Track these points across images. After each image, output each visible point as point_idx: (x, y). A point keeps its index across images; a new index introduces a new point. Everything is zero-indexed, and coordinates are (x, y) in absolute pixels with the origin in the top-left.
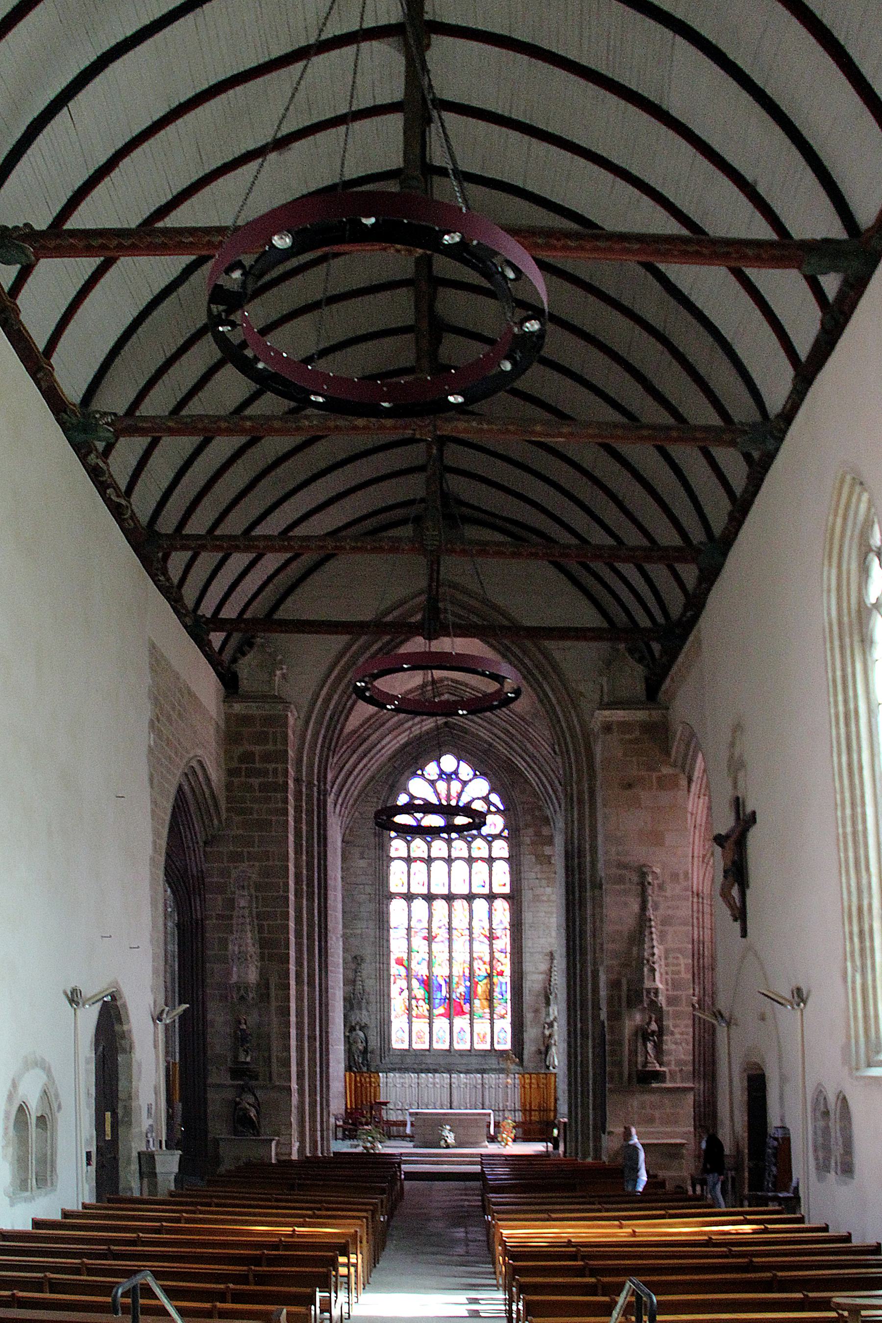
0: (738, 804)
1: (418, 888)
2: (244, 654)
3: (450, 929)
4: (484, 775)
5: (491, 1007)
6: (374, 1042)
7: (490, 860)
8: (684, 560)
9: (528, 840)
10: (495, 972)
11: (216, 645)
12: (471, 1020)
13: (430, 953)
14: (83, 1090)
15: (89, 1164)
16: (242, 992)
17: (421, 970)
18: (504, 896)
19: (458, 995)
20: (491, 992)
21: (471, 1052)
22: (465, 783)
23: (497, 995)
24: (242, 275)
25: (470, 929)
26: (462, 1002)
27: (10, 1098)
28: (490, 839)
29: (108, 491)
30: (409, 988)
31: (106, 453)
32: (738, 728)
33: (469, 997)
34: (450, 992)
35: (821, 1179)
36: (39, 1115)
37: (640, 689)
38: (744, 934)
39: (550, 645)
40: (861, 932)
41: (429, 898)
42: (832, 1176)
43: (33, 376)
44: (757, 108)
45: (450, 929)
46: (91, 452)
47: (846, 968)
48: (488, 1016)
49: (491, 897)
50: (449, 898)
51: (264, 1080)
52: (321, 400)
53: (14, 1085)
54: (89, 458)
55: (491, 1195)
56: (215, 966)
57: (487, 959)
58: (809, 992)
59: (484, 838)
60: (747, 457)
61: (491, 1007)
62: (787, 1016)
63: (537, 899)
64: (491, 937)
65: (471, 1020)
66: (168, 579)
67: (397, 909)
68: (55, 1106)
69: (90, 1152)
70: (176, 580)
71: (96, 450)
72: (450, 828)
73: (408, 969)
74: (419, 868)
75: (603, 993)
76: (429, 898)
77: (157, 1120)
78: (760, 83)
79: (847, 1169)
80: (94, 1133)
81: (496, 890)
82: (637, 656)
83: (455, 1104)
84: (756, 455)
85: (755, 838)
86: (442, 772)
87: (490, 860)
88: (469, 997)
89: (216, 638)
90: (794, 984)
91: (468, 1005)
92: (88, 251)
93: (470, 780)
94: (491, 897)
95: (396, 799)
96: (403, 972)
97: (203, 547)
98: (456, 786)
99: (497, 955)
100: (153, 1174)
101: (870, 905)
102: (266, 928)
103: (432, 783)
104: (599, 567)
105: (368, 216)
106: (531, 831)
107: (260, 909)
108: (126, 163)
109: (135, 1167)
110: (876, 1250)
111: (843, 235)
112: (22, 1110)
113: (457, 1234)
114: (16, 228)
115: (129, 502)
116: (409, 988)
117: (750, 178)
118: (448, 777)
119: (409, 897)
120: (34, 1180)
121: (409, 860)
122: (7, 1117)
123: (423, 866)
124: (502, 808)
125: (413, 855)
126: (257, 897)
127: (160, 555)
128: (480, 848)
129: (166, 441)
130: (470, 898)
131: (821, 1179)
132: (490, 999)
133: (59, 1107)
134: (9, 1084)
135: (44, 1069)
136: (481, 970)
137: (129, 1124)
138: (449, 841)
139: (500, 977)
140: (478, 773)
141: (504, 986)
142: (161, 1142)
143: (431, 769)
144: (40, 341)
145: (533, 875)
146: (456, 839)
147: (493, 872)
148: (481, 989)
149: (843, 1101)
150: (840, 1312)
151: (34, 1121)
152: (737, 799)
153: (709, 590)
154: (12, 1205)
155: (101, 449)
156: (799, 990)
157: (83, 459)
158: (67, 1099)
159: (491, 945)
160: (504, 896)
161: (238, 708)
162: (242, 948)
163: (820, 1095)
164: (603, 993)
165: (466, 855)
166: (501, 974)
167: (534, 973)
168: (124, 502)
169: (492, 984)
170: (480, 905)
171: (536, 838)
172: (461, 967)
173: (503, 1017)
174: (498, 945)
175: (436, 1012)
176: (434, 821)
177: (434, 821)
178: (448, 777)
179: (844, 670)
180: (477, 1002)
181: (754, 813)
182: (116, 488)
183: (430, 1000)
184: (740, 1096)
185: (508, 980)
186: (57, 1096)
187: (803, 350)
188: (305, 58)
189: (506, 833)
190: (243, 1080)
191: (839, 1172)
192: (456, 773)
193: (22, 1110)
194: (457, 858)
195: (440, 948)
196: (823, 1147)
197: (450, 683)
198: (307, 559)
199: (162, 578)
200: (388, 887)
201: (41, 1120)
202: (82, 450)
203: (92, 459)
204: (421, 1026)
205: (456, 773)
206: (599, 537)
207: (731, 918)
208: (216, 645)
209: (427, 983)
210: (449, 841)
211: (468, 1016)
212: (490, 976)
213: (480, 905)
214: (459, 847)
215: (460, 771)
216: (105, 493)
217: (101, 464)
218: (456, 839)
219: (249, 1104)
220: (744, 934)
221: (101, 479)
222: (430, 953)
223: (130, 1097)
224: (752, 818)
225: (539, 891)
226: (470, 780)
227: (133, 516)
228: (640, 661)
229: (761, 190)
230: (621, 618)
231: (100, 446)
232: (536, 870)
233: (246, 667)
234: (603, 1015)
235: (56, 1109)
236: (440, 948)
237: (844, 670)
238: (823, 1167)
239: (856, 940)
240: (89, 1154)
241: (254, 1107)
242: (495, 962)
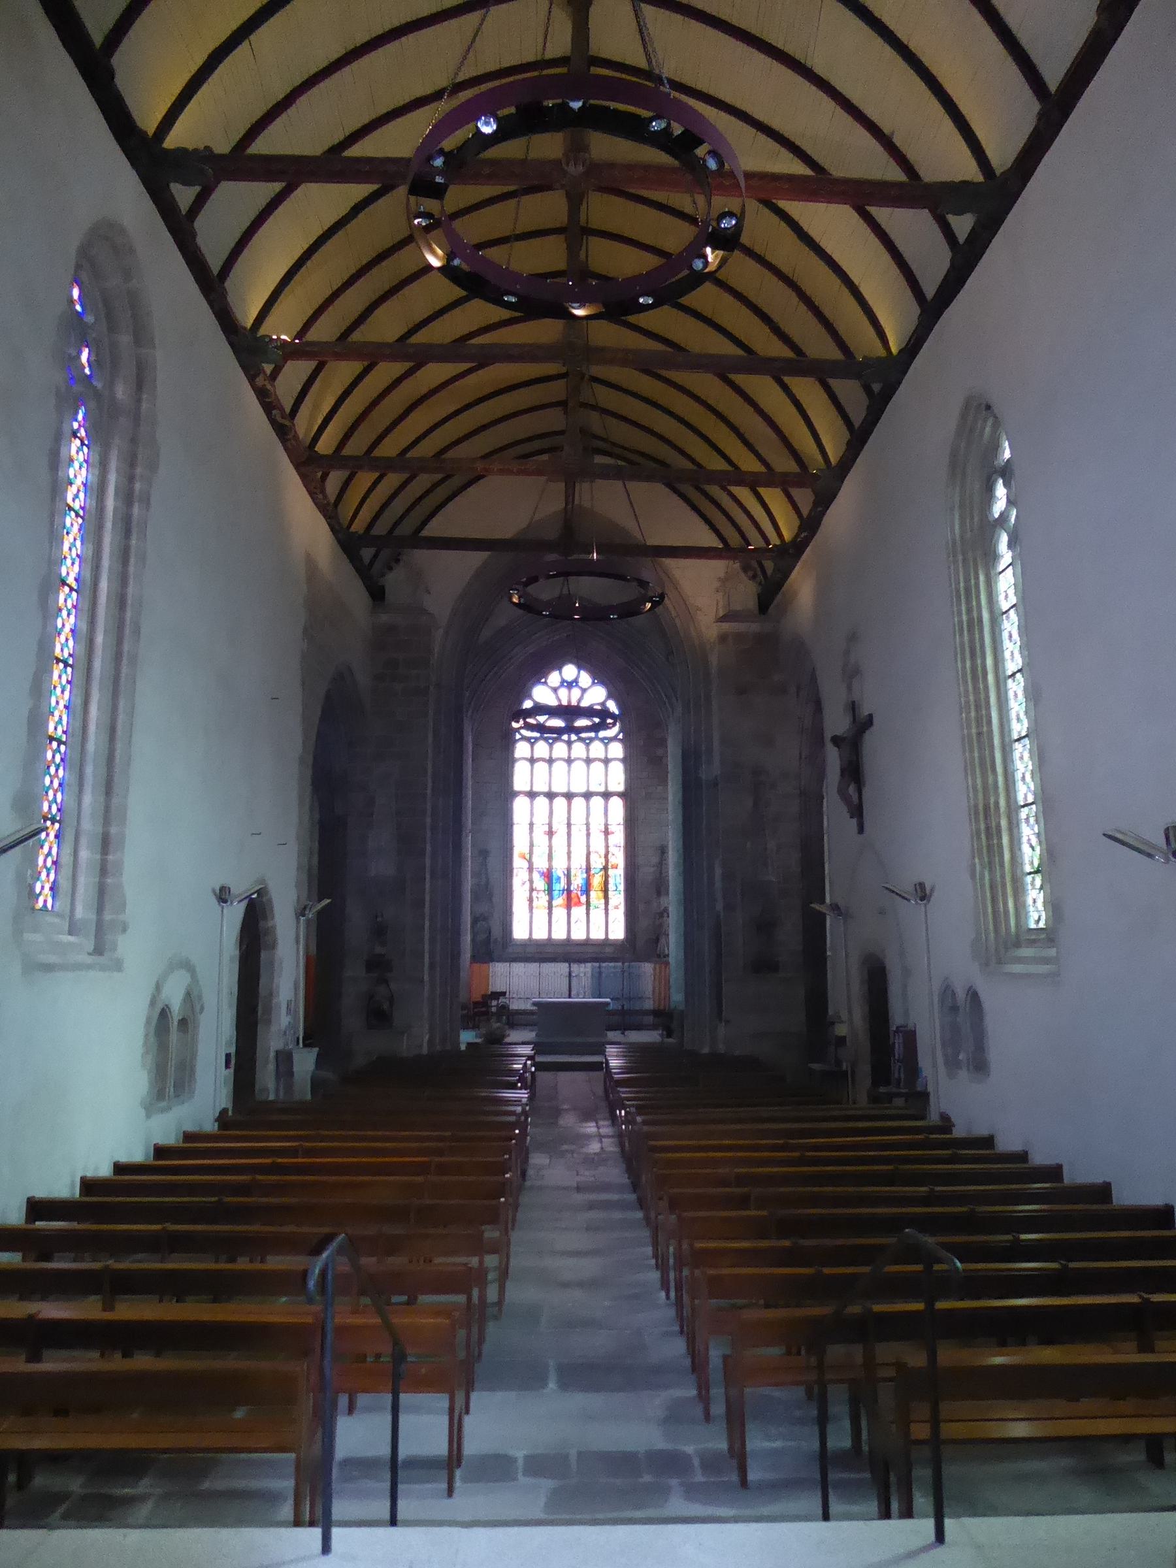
0: (853, 707)
1: (557, 788)
2: (391, 569)
3: (569, 825)
4: (602, 683)
5: (606, 897)
6: (496, 932)
7: (606, 761)
8: (800, 485)
10: (610, 865)
11: (367, 560)
12: (588, 909)
13: (550, 847)
14: (225, 991)
15: (227, 1066)
17: (541, 863)
18: (620, 795)
19: (576, 887)
20: (606, 883)
21: (587, 943)
22: (584, 691)
23: (611, 887)
24: (444, 163)
25: (588, 825)
26: (579, 893)
27: (153, 1003)
28: (606, 741)
29: (274, 412)
30: (531, 881)
31: (274, 376)
32: (853, 638)
33: (587, 888)
34: (569, 883)
35: (951, 1075)
36: (181, 1018)
37: (752, 604)
38: (861, 830)
39: (670, 563)
40: (988, 829)
41: (551, 796)
42: (963, 1074)
43: (206, 296)
44: (899, 61)
45: (569, 825)
46: (259, 374)
47: (974, 865)
48: (603, 906)
49: (607, 795)
50: (569, 796)
52: (513, 300)
53: (158, 987)
54: (257, 379)
55: (621, 1090)
57: (603, 853)
58: (932, 890)
59: (602, 740)
60: (868, 389)
61: (606, 897)
62: (911, 911)
64: (607, 832)
65: (588, 909)
66: (325, 497)
67: (520, 806)
68: (198, 1008)
69: (230, 1054)
70: (332, 499)
71: (264, 372)
72: (570, 729)
73: (530, 862)
74: (541, 767)
75: (718, 884)
76: (551, 796)
77: (296, 1018)
78: (904, 40)
79: (980, 1066)
80: (235, 1033)
81: (611, 789)
82: (750, 573)
83: (573, 993)
84: (876, 387)
85: (871, 740)
86: (563, 681)
87: (606, 761)
88: (587, 888)
89: (367, 553)
90: (916, 880)
91: (585, 896)
92: (269, 177)
93: (589, 688)
94: (607, 795)
95: (521, 703)
96: (526, 865)
97: (360, 468)
98: (576, 693)
100: (290, 1073)
101: (997, 803)
103: (555, 690)
104: (715, 491)
105: (577, 99)
108: (303, 101)
109: (271, 1067)
110: (1160, 1216)
111: (980, 178)
112: (164, 1014)
113: (515, 1066)
114: (196, 150)
115: (293, 423)
116: (531, 881)
117: (886, 131)
118: (570, 685)
119: (532, 795)
120: (172, 1090)
121: (532, 761)
122: (148, 1022)
123: (545, 765)
125: (536, 756)
127: (320, 474)
128: (597, 749)
129: (331, 365)
130: (588, 796)
131: (951, 1075)
132: (605, 891)
133: (202, 1009)
134: (153, 985)
135: (188, 971)
136: (597, 863)
137: (268, 1022)
138: (569, 743)
140: (543, 680)
141: (618, 878)
142: (298, 1039)
143: (554, 678)
144: (215, 264)
146: (575, 741)
148: (597, 881)
149: (974, 996)
150: (1014, 1234)
151: (176, 1023)
152: (853, 703)
153: (823, 513)
154: (148, 1116)
155: (268, 372)
156: (922, 885)
157: (251, 379)
158: (210, 999)
159: (606, 840)
160: (620, 795)
161: (384, 618)
163: (947, 991)
164: (718, 884)
165: (602, 756)
168: (287, 423)
169: (607, 877)
170: (597, 802)
172: (579, 862)
173: (616, 907)
174: (612, 840)
175: (555, 903)
176: (558, 723)
177: (558, 723)
178: (570, 685)
179: (967, 581)
180: (593, 894)
181: (870, 716)
182: (282, 409)
183: (550, 891)
184: (857, 988)
186: (200, 997)
187: (930, 291)
188: (482, 8)
189: (621, 736)
191: (971, 1067)
192: (576, 681)
193: (164, 1014)
194: (576, 759)
195: (560, 840)
196: (952, 1040)
198: (456, 482)
199: (320, 496)
200: (512, 787)
201: (183, 1022)
202: (251, 372)
203: (260, 381)
204: (541, 914)
205: (576, 681)
206: (720, 465)
207: (848, 815)
208: (367, 560)
209: (548, 876)
210: (569, 743)
211: (585, 907)
212: (605, 869)
213: (597, 802)
214: (579, 749)
215: (580, 680)
216: (271, 413)
217: (269, 387)
218: (575, 741)
220: (861, 830)
221: (267, 400)
222: (550, 847)
223: (271, 994)
224: (869, 721)
226: (589, 688)
227: (296, 437)
228: (754, 577)
229: (897, 141)
230: (735, 540)
231: (268, 368)
233: (394, 581)
234: (719, 906)
235: (198, 1011)
236: (560, 840)
237: (967, 581)
238: (953, 1064)
239: (983, 837)
240: (228, 1056)
242: (610, 855)
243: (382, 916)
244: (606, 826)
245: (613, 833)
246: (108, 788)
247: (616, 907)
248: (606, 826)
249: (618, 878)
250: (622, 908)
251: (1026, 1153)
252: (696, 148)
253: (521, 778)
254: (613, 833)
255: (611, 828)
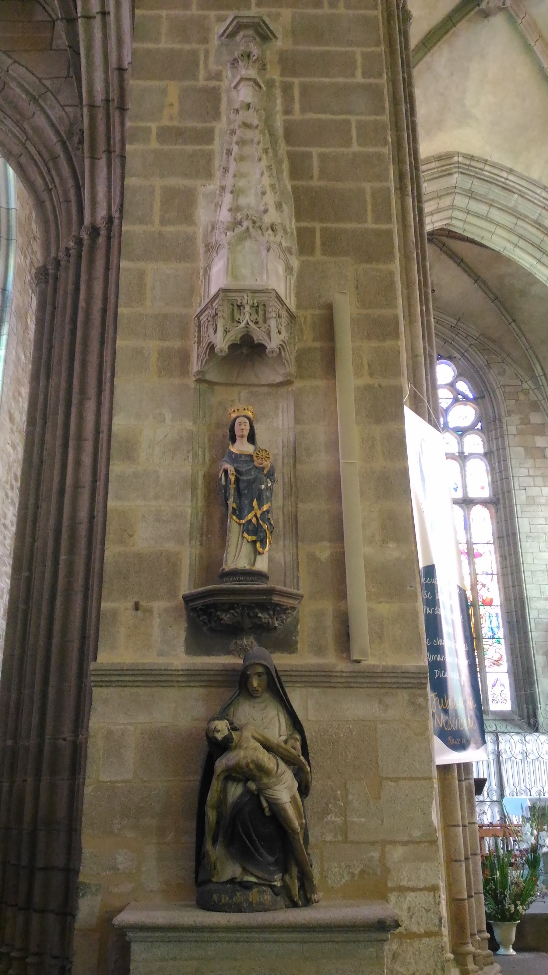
9: (513, 429)
16: (246, 317)
18: (484, 503)
51: (319, 650)
56: (150, 267)
63: (532, 501)
81: (473, 494)
99: (480, 578)
102: (315, 162)
106: (515, 419)
107: (297, 115)
124: (471, 396)
126: (287, 89)
139: (487, 608)
141: (494, 620)
145: (524, 471)
147: (468, 474)
160: (484, 503)
162: (243, 201)
166: (489, 603)
167: (539, 598)
171: (523, 427)
173: (497, 663)
185: (498, 610)
189: (479, 426)
190: (243, 651)
197: (461, 159)
219: (268, 747)
225: (534, 491)
232: (526, 465)
241: (289, 761)
243: (251, 438)
244: (470, 544)
245: (481, 555)
246: (499, 209)
247: (497, 663)
248: (470, 544)
249: (494, 620)
250: (505, 666)
251: (454, 503)
252: (78, 878)
253: (484, 643)
254: (481, 555)
255: (477, 548)
